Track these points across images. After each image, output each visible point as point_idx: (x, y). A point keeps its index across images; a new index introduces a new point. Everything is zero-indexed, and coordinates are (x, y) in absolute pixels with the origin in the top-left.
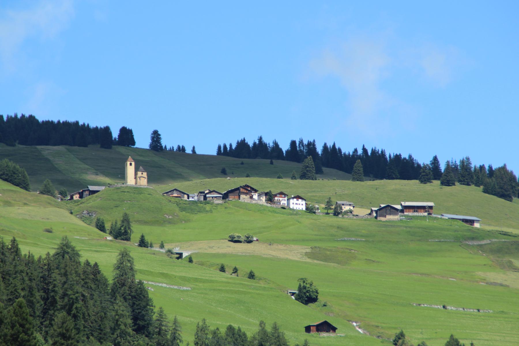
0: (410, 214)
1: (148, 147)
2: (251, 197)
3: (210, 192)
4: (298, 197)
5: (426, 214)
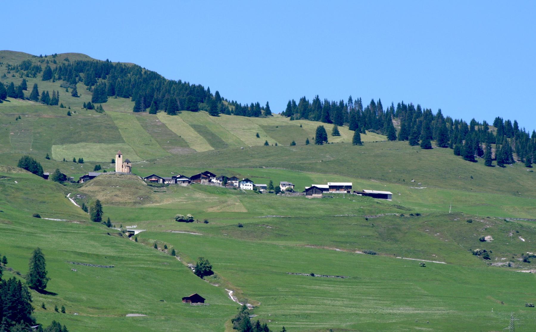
0: (334, 191)
1: (354, 132)
2: (210, 181)
3: (181, 177)
4: (247, 181)
5: (346, 192)
